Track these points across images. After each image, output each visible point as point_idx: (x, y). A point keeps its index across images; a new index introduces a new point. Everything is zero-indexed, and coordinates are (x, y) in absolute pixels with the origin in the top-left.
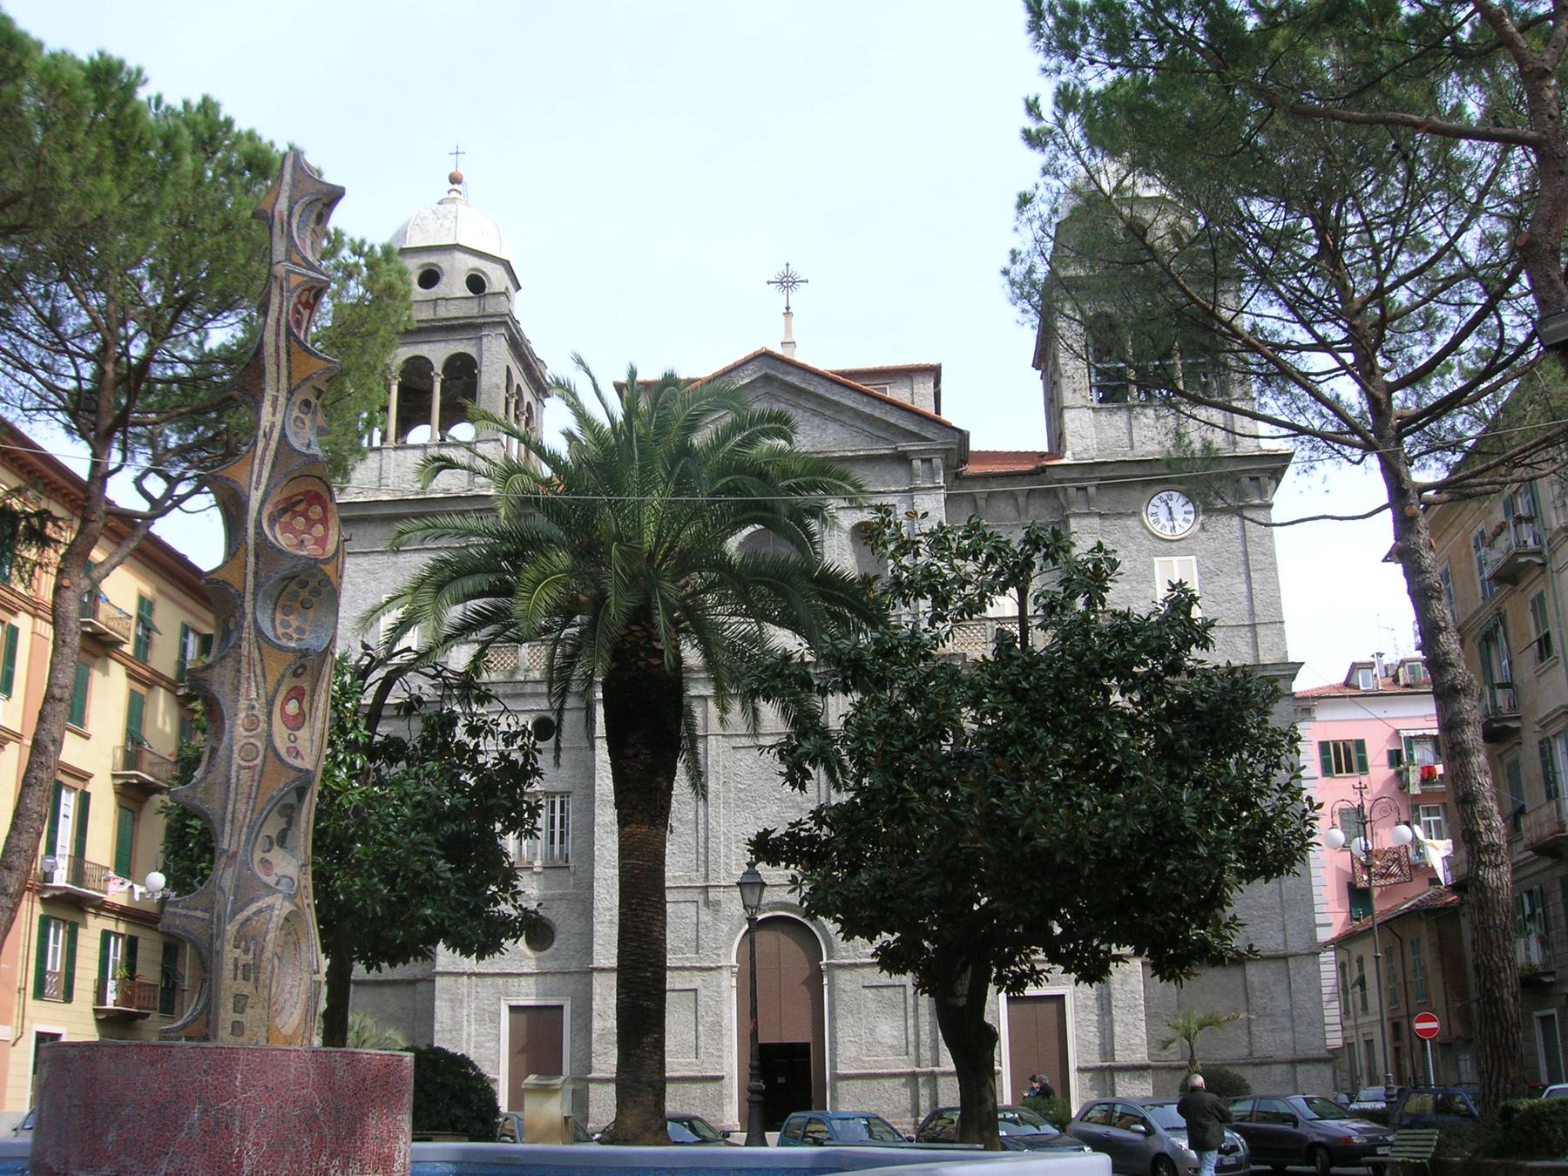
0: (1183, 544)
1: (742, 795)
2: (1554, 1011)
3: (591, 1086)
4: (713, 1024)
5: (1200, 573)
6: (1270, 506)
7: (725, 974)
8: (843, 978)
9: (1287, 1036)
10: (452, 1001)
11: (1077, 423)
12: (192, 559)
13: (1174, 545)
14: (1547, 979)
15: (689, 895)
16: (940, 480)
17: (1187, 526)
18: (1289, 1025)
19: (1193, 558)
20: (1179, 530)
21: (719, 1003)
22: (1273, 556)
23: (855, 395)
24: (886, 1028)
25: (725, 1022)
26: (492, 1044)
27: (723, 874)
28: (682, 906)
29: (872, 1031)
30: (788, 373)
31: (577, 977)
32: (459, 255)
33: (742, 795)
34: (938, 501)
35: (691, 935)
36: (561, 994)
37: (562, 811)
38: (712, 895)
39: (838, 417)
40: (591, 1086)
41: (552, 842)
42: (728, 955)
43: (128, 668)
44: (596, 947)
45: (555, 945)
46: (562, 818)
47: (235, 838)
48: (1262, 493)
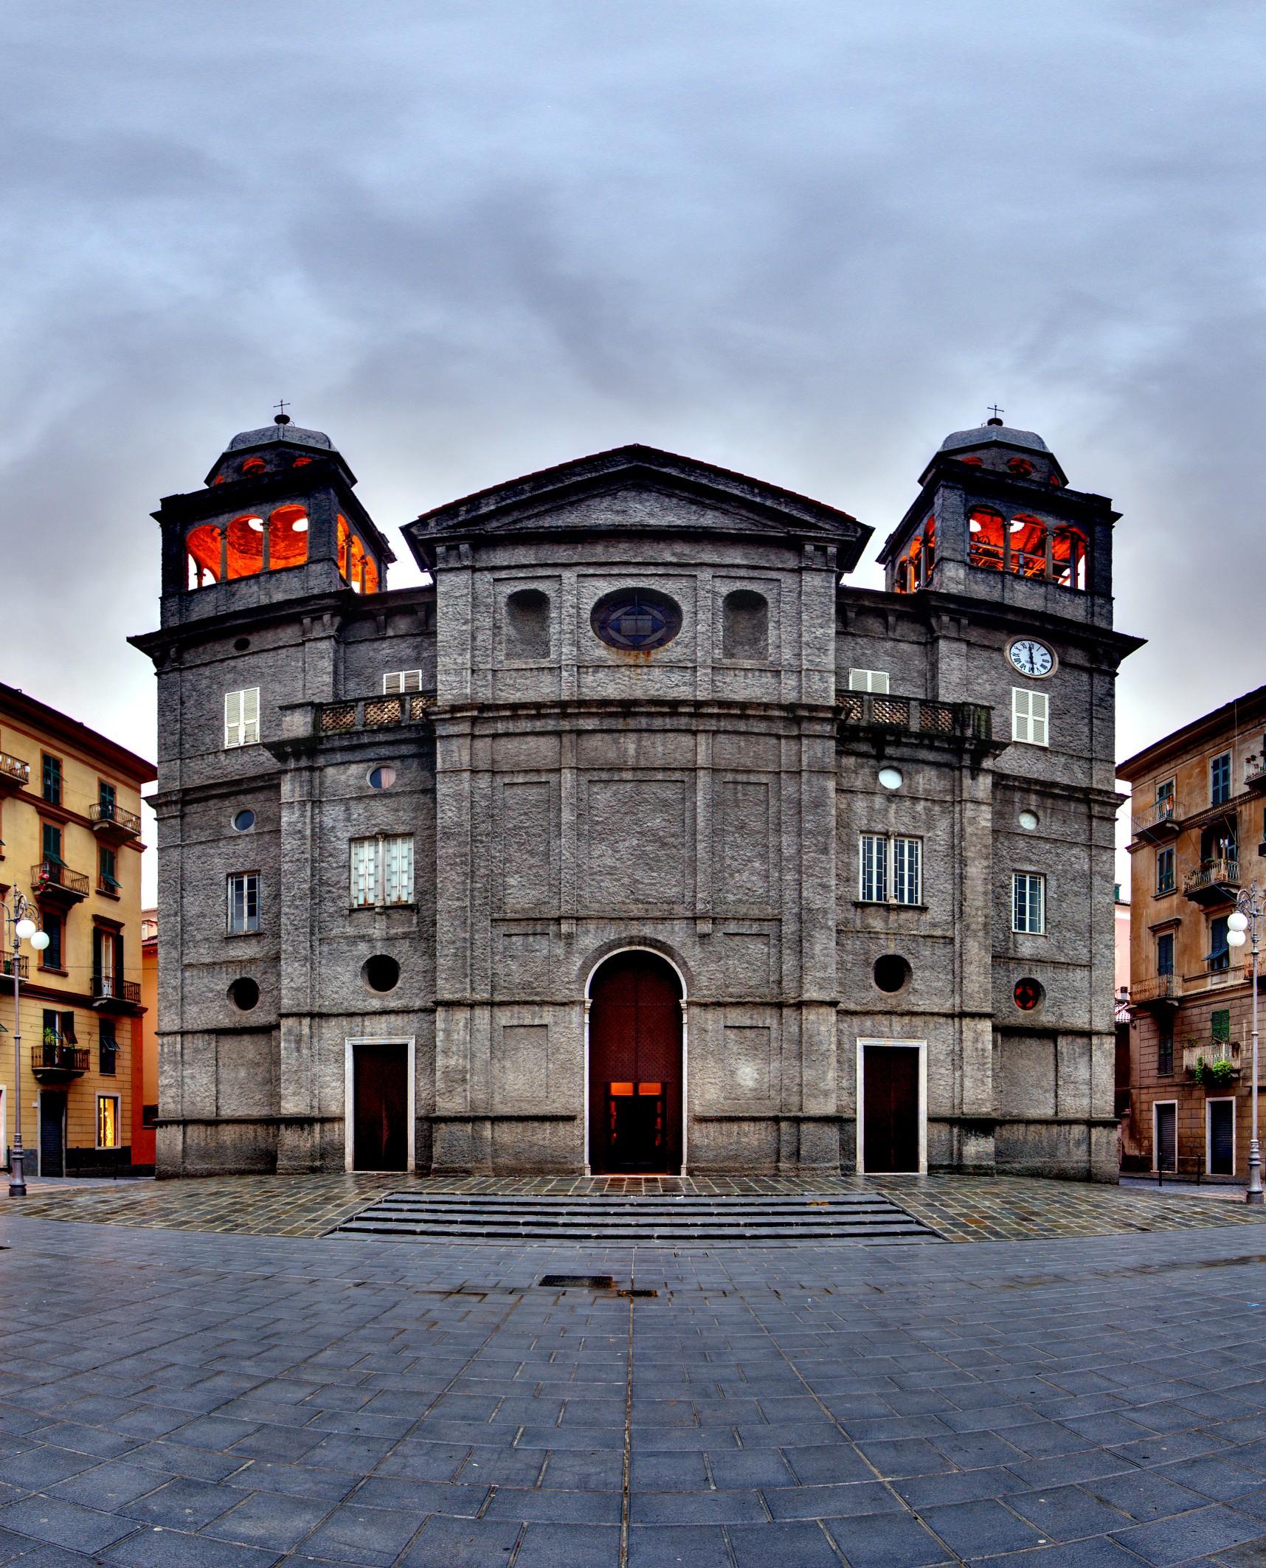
2: (1233, 1098)
9: (1086, 1101)
12: (87, 725)
14: (1235, 1075)
17: (1043, 671)
18: (1087, 1092)
19: (1047, 696)
20: (1036, 672)
29: (733, 1073)
31: (421, 1015)
39: (719, 505)
43: (37, 807)
45: (399, 984)
47: (560, 1220)
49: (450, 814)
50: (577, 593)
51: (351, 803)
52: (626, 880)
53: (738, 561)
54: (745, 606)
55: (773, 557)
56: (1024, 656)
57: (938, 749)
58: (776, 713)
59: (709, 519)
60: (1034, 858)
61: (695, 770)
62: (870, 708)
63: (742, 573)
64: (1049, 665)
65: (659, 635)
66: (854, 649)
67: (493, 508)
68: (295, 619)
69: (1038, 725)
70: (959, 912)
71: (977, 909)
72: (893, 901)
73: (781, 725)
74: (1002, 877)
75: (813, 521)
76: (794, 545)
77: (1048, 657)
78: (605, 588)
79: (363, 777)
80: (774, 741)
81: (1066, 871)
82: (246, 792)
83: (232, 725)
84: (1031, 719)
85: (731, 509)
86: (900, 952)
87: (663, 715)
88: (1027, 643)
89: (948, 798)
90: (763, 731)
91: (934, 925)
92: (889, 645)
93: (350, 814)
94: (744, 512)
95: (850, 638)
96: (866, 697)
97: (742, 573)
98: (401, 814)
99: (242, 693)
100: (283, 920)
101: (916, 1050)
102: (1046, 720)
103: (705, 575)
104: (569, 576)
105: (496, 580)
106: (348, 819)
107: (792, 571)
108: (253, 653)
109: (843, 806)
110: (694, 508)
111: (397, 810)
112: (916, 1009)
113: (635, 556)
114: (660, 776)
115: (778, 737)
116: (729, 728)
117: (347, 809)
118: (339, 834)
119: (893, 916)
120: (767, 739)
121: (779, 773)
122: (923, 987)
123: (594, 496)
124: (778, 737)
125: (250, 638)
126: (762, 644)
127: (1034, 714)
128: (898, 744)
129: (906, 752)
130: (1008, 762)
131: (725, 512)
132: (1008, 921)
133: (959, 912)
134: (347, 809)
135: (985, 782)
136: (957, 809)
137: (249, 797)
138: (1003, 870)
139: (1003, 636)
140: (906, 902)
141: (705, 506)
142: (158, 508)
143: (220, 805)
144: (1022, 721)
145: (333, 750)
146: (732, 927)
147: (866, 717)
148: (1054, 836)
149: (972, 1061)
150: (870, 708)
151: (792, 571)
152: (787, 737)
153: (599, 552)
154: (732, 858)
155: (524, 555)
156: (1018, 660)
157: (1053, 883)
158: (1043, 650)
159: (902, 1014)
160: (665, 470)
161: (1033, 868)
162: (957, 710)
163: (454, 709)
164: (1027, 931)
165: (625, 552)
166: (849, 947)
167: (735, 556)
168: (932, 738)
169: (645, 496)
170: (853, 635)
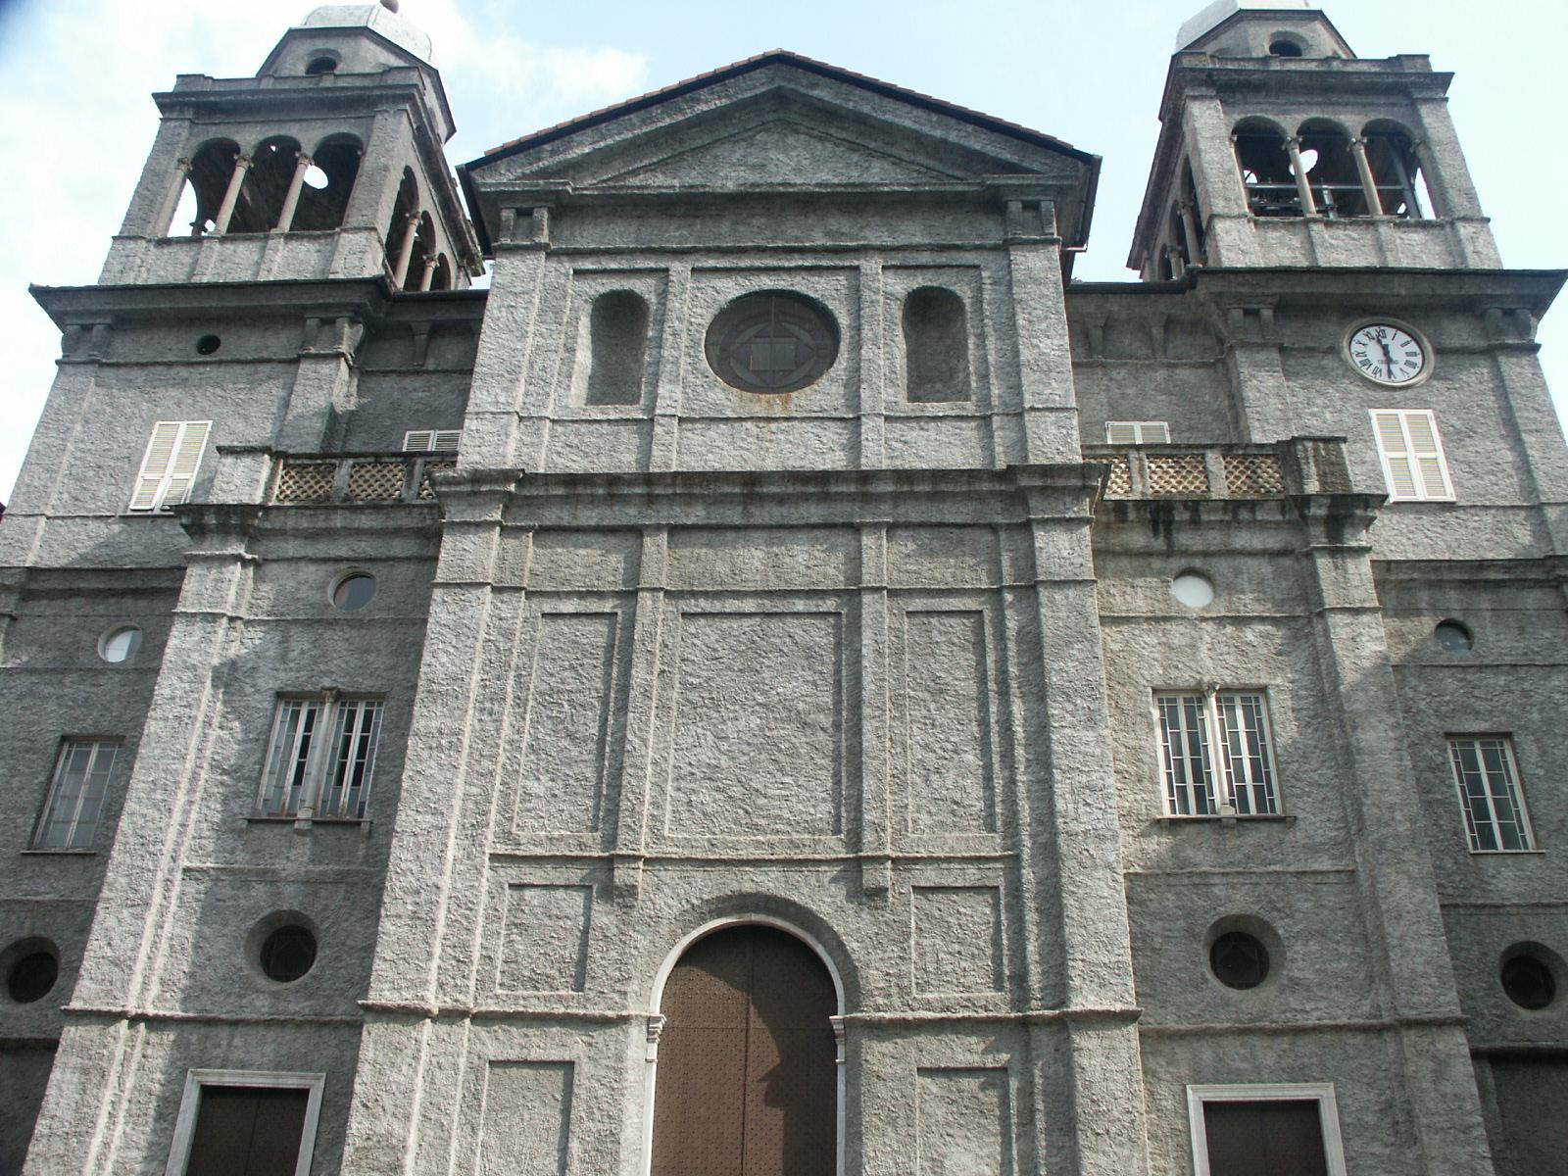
0: (1410, 393)
1: (693, 696)
3: (1079, 1040)
4: (600, 1138)
5: (1443, 433)
6: (1536, 348)
7: (636, 1033)
8: (878, 1054)
10: (85, 1071)
11: (1235, 235)
13: (1398, 395)
15: (575, 874)
16: (1054, 230)
19: (1429, 413)
21: (616, 1092)
22: (1552, 413)
23: (920, 112)
24: (966, 1159)
25: (628, 1135)
26: (1348, 1120)
27: (645, 836)
28: (560, 894)
30: (815, 86)
32: (366, 44)
33: (693, 696)
34: (1050, 259)
35: (571, 952)
36: (307, 1066)
37: (366, 728)
38: (621, 875)
39: (889, 150)
40: (1079, 1040)
41: (340, 781)
42: (643, 996)
44: (378, 965)
46: (364, 741)
48: (1527, 330)
49: (444, 659)
50: (692, 302)
51: (294, 631)
52: (737, 791)
53: (917, 240)
54: (930, 313)
55: (966, 230)
56: (1374, 353)
57: (1264, 525)
58: (986, 486)
59: (879, 175)
60: (1481, 706)
61: (859, 592)
62: (1141, 469)
63: (925, 258)
64: (1418, 360)
65: (806, 368)
66: (1108, 390)
67: (587, 150)
68: (293, 317)
69: (1429, 464)
70: (1354, 823)
71: (1391, 808)
72: (1229, 812)
73: (998, 506)
74: (1428, 751)
75: (1015, 159)
76: (992, 204)
77: (1413, 347)
78: (731, 289)
79: (322, 588)
80: (988, 537)
81: (1549, 722)
82: (137, 593)
83: (149, 476)
84: (1413, 456)
85: (904, 156)
86: (1254, 909)
87: (805, 498)
88: (1373, 331)
89: (1299, 611)
90: (968, 519)
91: (1314, 850)
92: (1160, 375)
93: (286, 651)
94: (921, 159)
95: (1099, 371)
96: (1133, 455)
97: (925, 258)
98: (371, 658)
99: (183, 425)
100: (124, 824)
101: (1313, 1106)
102: (1440, 454)
103: (871, 265)
104: (679, 268)
105: (576, 272)
106: (283, 658)
107: (994, 248)
108: (220, 363)
109: (1116, 647)
110: (855, 157)
111: (367, 651)
112: (1302, 1020)
113: (774, 238)
114: (800, 605)
115: (993, 528)
116: (914, 517)
117: (285, 640)
118: (260, 682)
119: (1232, 842)
120: (976, 533)
121: (999, 592)
122: (1310, 975)
123: (722, 141)
124: (993, 528)
125: (222, 337)
126: (961, 375)
127: (1418, 447)
128: (1195, 523)
129: (1214, 539)
130: (1390, 538)
131: (897, 161)
132: (1457, 833)
133: (1354, 823)
134: (285, 640)
135: (1361, 570)
136: (1319, 627)
137: (142, 604)
138: (1427, 736)
139: (1333, 328)
140: (1253, 811)
141: (871, 153)
142: (169, 86)
143: (87, 610)
144: (1400, 466)
145: (282, 533)
146: (929, 876)
147: (1138, 487)
148: (1508, 660)
149: (1440, 1122)
150: (1141, 469)
151: (994, 248)
152: (1009, 527)
153: (725, 232)
154: (927, 747)
155: (621, 234)
156: (1367, 363)
157: (1530, 749)
158: (1402, 337)
159: (1275, 1033)
160: (816, 93)
161: (1481, 726)
162: (1285, 453)
163: (478, 477)
164: (1501, 848)
165: (761, 231)
166: (1153, 907)
167: (913, 232)
168: (1252, 505)
169: (790, 140)
170: (1104, 366)
